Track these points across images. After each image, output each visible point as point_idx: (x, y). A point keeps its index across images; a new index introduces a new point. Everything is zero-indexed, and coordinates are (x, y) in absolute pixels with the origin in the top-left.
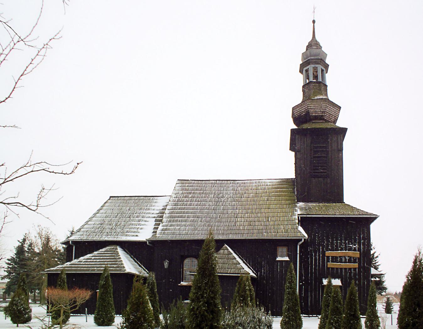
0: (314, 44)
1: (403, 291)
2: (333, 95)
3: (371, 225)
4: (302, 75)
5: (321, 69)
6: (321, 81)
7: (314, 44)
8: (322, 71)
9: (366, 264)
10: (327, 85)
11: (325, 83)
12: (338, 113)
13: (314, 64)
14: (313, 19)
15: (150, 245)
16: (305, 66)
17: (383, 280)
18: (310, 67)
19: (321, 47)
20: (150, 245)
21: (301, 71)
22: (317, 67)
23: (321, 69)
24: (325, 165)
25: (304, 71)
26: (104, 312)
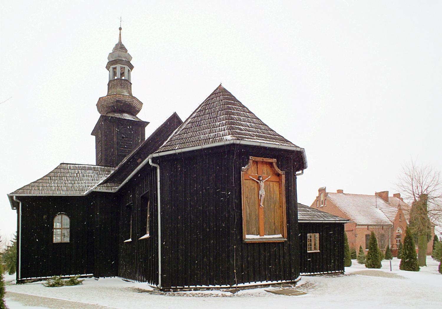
0: (120, 47)
1: (381, 263)
2: (136, 92)
3: (146, 128)
4: (108, 72)
5: (128, 69)
6: (127, 79)
7: (120, 47)
8: (129, 71)
9: (126, 204)
10: (131, 83)
11: (130, 82)
12: (141, 109)
13: (120, 62)
14: (120, 27)
15: (148, 232)
16: (161, 188)
17: (4, 300)
18: (118, 66)
19: (126, 51)
20: (148, 232)
21: (108, 67)
22: (124, 68)
23: (128, 69)
24: (130, 147)
25: (111, 69)
26: (177, 218)
